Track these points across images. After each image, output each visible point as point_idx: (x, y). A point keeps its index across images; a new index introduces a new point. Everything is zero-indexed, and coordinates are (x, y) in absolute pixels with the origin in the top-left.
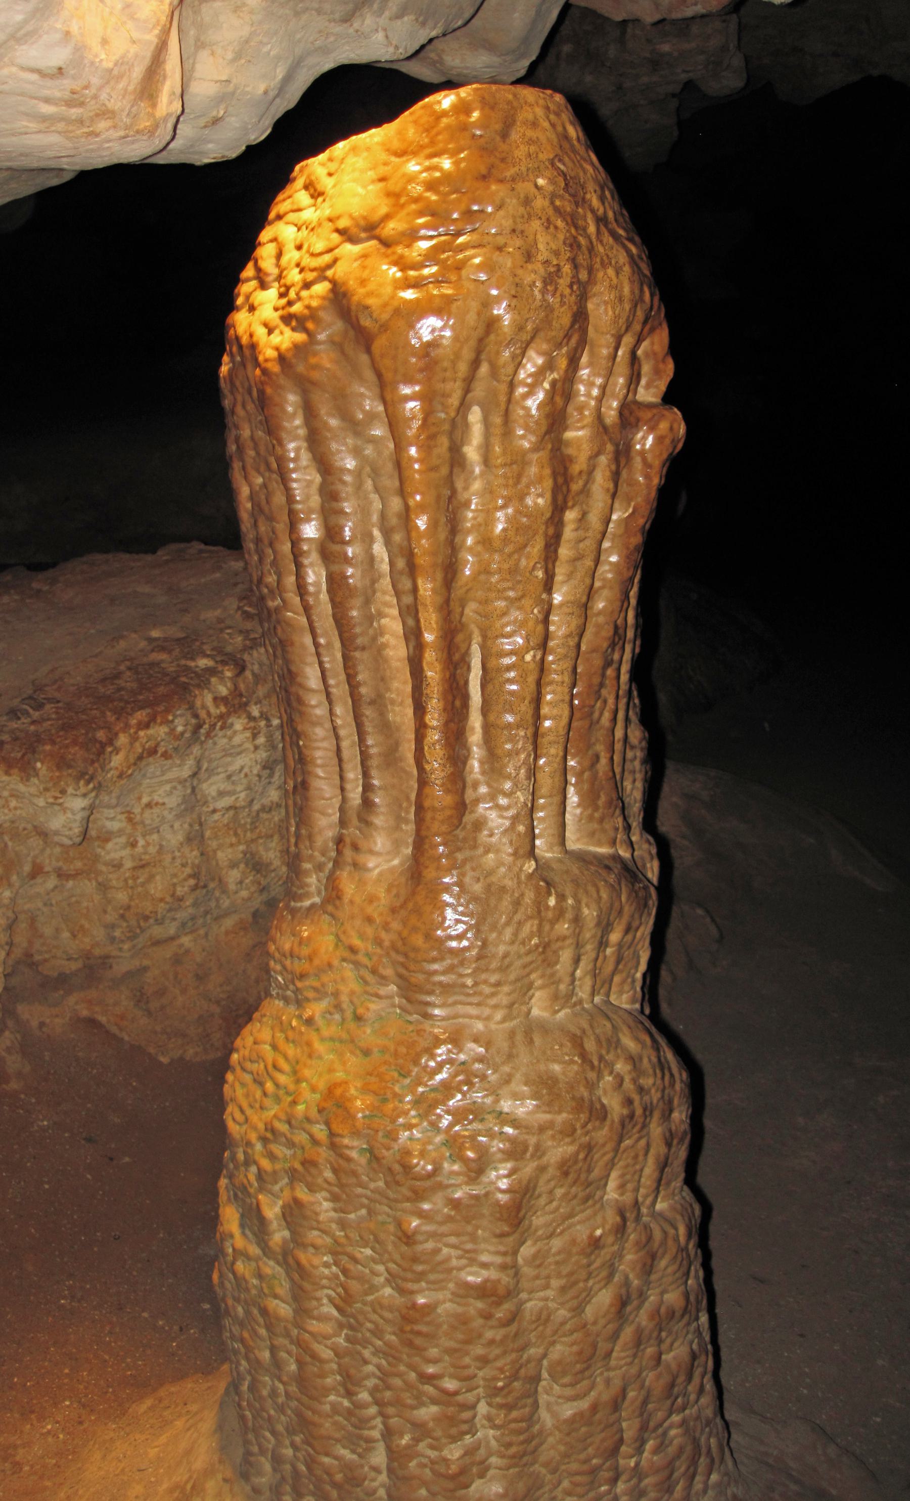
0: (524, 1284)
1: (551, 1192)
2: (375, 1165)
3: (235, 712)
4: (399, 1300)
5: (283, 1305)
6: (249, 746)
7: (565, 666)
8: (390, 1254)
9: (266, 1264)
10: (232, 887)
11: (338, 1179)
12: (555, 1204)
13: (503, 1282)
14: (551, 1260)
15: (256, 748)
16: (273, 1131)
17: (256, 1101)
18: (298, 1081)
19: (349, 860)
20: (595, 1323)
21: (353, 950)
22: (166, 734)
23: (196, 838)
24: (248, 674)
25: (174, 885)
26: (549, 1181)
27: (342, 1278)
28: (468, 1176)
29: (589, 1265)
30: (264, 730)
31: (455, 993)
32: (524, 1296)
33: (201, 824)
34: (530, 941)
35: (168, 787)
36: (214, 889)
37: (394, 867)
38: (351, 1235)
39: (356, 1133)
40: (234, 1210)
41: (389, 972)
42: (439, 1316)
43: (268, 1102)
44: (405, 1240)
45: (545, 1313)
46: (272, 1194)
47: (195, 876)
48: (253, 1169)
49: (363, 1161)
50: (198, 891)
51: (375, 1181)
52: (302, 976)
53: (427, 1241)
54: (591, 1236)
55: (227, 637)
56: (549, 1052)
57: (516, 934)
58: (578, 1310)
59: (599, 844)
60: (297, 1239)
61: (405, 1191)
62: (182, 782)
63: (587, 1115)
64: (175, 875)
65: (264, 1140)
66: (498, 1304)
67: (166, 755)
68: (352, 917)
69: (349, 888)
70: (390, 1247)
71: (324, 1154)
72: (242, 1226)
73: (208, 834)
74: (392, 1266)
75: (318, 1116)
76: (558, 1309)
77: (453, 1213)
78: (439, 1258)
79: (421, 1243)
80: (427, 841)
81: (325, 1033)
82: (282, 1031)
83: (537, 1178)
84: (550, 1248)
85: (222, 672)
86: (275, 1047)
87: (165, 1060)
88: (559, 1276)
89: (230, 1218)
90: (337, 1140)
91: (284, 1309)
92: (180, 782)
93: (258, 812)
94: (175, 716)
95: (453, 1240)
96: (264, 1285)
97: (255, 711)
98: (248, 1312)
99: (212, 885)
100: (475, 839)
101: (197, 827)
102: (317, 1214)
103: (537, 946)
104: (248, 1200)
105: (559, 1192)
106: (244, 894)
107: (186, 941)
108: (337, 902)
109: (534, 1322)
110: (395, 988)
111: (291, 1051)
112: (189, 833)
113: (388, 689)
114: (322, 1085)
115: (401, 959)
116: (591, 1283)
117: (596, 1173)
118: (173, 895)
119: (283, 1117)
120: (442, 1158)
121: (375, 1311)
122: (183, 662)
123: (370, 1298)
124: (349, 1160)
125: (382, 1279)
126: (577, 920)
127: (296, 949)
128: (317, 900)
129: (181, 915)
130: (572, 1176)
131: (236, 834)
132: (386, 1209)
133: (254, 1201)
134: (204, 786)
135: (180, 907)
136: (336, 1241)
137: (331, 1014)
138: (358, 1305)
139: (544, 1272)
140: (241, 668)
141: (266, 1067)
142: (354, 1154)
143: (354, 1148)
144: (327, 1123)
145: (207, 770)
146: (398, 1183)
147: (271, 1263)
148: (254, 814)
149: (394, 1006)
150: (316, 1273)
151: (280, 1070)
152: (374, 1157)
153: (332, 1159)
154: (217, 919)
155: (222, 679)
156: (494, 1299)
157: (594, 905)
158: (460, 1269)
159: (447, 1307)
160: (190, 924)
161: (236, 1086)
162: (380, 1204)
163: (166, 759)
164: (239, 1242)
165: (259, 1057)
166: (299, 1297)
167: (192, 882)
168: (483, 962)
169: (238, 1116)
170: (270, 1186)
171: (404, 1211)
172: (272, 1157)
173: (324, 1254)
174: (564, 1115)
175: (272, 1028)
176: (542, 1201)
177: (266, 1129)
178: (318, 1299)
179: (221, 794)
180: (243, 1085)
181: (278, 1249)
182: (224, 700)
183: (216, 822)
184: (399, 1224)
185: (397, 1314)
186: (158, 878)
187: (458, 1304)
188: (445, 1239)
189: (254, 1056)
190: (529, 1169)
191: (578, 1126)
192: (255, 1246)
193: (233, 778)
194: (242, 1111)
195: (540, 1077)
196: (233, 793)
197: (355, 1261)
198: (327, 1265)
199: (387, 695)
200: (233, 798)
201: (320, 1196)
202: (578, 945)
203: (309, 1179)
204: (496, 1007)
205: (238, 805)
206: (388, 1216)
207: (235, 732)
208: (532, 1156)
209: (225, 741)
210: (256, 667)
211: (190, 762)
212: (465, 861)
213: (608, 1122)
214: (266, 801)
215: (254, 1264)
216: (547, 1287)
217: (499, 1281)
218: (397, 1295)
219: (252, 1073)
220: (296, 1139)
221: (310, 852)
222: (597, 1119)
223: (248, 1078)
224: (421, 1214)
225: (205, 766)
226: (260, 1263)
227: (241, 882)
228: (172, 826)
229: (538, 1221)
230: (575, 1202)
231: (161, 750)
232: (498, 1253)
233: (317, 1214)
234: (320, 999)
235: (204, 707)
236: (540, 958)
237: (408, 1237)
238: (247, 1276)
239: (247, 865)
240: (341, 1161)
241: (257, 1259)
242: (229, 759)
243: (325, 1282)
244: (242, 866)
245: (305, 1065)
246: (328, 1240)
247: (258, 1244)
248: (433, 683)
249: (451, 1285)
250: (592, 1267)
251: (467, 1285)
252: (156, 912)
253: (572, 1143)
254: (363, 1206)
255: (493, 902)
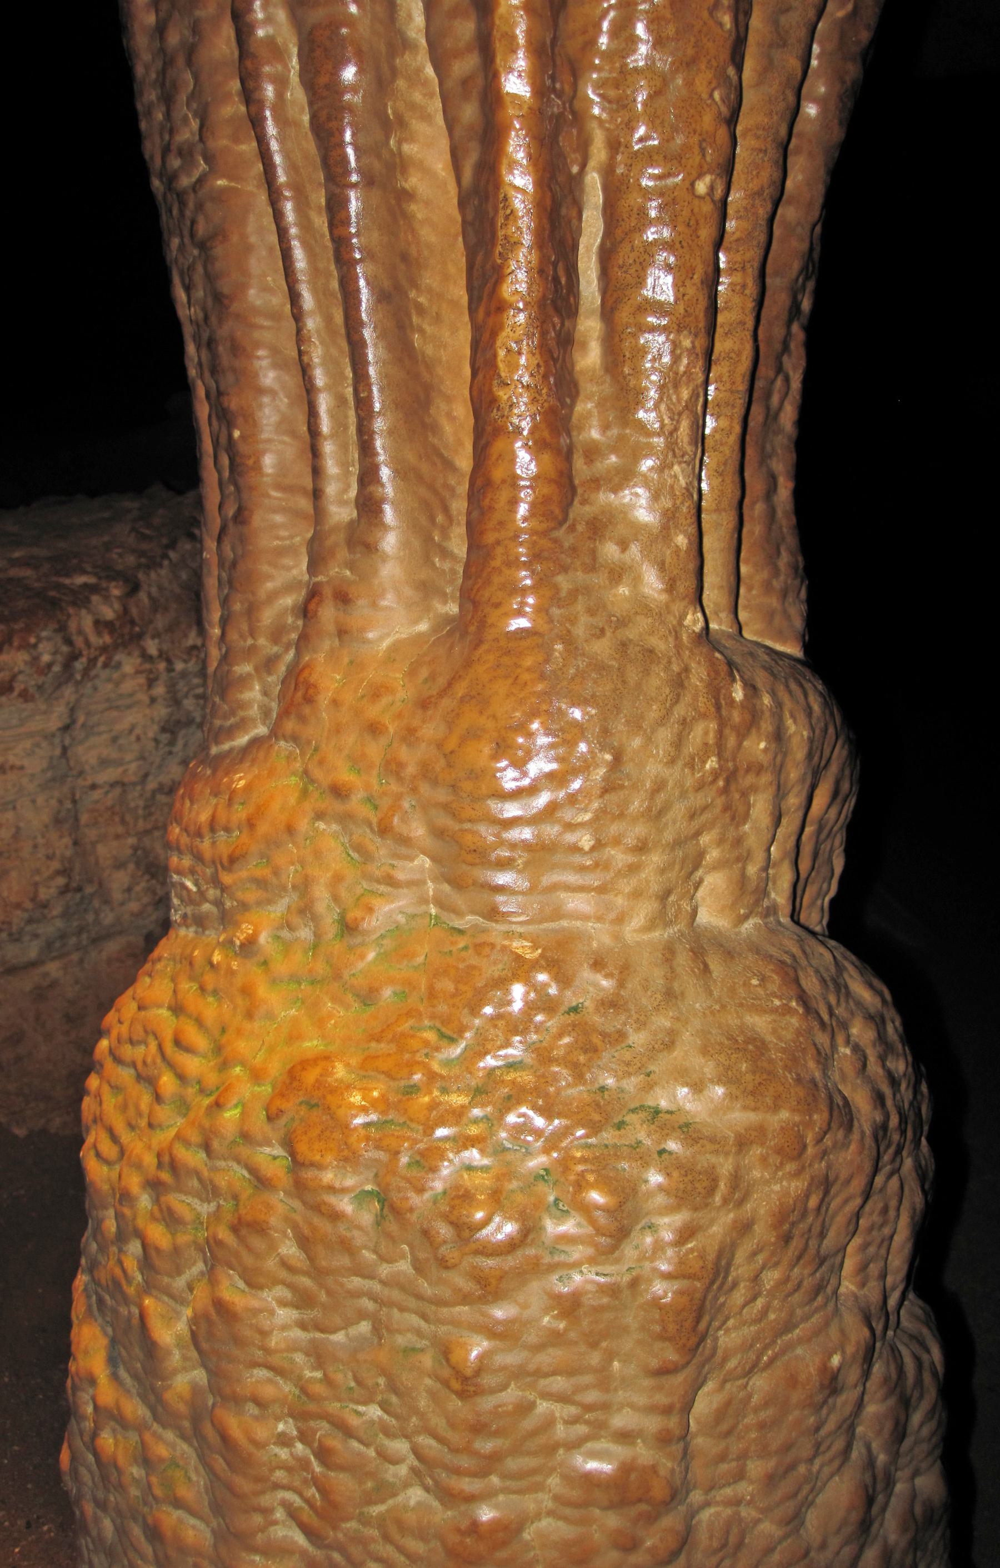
0: (698, 1471)
1: (756, 1278)
2: (393, 1227)
3: (125, 645)
4: (441, 1515)
5: (192, 1521)
6: (143, 697)
7: (749, 255)
8: (421, 1415)
9: (159, 1438)
10: (117, 896)
11: (311, 1259)
12: (760, 1302)
13: (662, 1472)
14: (750, 1419)
15: (153, 700)
16: (174, 1167)
17: (140, 1114)
18: (224, 1066)
19: (331, 627)
20: (823, 1546)
21: (339, 792)
22: (26, 663)
23: (66, 820)
24: (143, 595)
25: (36, 884)
26: (754, 1254)
27: (318, 1469)
28: (596, 1245)
29: (817, 1429)
30: (164, 676)
31: (554, 867)
32: (696, 1497)
33: (74, 802)
34: (704, 762)
35: (28, 744)
36: (92, 895)
37: (420, 635)
38: (339, 1377)
39: (349, 1159)
40: (98, 1331)
41: (418, 830)
42: (527, 1546)
43: (164, 1113)
44: (456, 1385)
45: (735, 1530)
46: (172, 1296)
47: (65, 872)
48: (135, 1247)
49: (367, 1218)
50: (69, 895)
51: (390, 1261)
52: (233, 861)
53: (504, 1387)
54: (824, 1368)
55: (115, 556)
56: (741, 991)
57: (678, 743)
58: (795, 1521)
59: (784, 641)
60: (222, 1387)
61: (460, 1281)
62: (49, 737)
63: (826, 1115)
64: (38, 871)
65: (155, 1186)
66: (651, 1519)
67: (25, 696)
68: (338, 730)
69: (329, 679)
70: (423, 1403)
71: (281, 1205)
72: (112, 1361)
73: (84, 818)
74: (425, 1441)
75: (267, 1128)
76: (758, 1521)
77: (562, 1326)
78: (528, 1424)
79: (493, 1391)
80: (499, 550)
81: (281, 967)
82: (192, 978)
83: (733, 1246)
84: (750, 1396)
85: (107, 589)
86: (177, 1009)
87: (20, 1132)
88: (764, 1452)
89: (91, 1345)
90: (308, 1174)
91: (195, 1531)
92: (45, 737)
93: (154, 793)
94: (39, 639)
95: (559, 1383)
96: (154, 1480)
97: (152, 647)
98: (121, 1531)
99: (89, 890)
100: (593, 553)
101: (68, 805)
102: (264, 1334)
103: (716, 774)
104: (123, 1311)
105: (771, 1277)
106: (134, 906)
107: (53, 968)
108: (307, 710)
109: (715, 1552)
110: (428, 863)
111: (210, 1010)
112: (59, 812)
113: (414, 284)
114: (276, 1068)
115: (442, 795)
116: (817, 1463)
117: (829, 1242)
118: (33, 900)
119: (195, 1137)
120: (539, 1204)
121: (387, 1538)
122: (54, 579)
123: (376, 1510)
124: (335, 1216)
125: (403, 1470)
126: (778, 736)
127: (222, 817)
128: (262, 730)
129: (49, 929)
130: (796, 1244)
131: (123, 821)
132: (415, 1320)
133: (135, 1311)
134: (80, 749)
135: (45, 917)
136: (303, 1390)
137: (291, 928)
138: (352, 1525)
139: (736, 1447)
140: (134, 588)
141: (160, 1048)
142: (346, 1205)
143: (347, 1190)
144: (289, 1144)
145: (83, 725)
146: (443, 1264)
147: (169, 1435)
148: (148, 795)
149: (424, 901)
150: (262, 1456)
151: (189, 1050)
152: (389, 1207)
153: (298, 1218)
154: (96, 941)
155: (107, 598)
156: (644, 1507)
157: (802, 717)
158: (574, 1445)
159: (547, 1528)
160: (57, 944)
161: (105, 1098)
162: (402, 1309)
163: (26, 701)
164: (106, 1393)
165: (146, 1032)
166: (225, 1503)
167: (61, 881)
168: (612, 797)
169: (107, 1148)
170: (166, 1280)
171: (455, 1323)
172: (171, 1219)
173: (278, 1419)
174: (784, 1115)
175: (174, 979)
176: (739, 1297)
177: (160, 1165)
178: (266, 1511)
179: (104, 763)
180: (116, 1089)
181: (182, 1408)
182: (109, 626)
183: (97, 802)
184: (445, 1351)
185: (436, 1544)
186: (14, 874)
187: (566, 1519)
188: (543, 1382)
189: (139, 1033)
190: (719, 1226)
191: (809, 1139)
192: (137, 1400)
193: (121, 741)
194: (114, 1138)
195: (731, 1038)
196: (119, 763)
197: (348, 1432)
198: (283, 1440)
199: (413, 294)
200: (120, 770)
201: (269, 1296)
202: (780, 793)
203: (249, 1260)
204: (636, 894)
205: (126, 780)
206: (419, 1333)
207: (124, 676)
208: (725, 1201)
209: (110, 686)
210: (154, 590)
211: (60, 710)
212: (574, 594)
213: (855, 1136)
214: (165, 779)
215: (134, 1437)
216: (740, 1475)
217: (654, 1469)
218: (436, 1504)
219: (134, 1065)
220: (222, 1181)
221: (250, 641)
222: (841, 1126)
223: (125, 1075)
224: (490, 1330)
225: (81, 719)
226: (148, 1437)
227: (129, 890)
228: (34, 801)
229: (728, 1338)
230: (797, 1297)
231: (18, 687)
232: (651, 1409)
233: (264, 1334)
234: (270, 902)
235: (80, 632)
236: (720, 802)
237: (465, 1379)
238: (121, 1461)
239: (138, 864)
240: (317, 1220)
241: (141, 1428)
242: (114, 714)
243: (279, 1475)
244: (131, 866)
245: (239, 1032)
246: (287, 1388)
247: (144, 1398)
248: (518, 203)
249: (554, 1481)
250: (823, 1432)
251: (589, 1480)
252: (10, 923)
253: (798, 1174)
254: (362, 1315)
255: (633, 675)
